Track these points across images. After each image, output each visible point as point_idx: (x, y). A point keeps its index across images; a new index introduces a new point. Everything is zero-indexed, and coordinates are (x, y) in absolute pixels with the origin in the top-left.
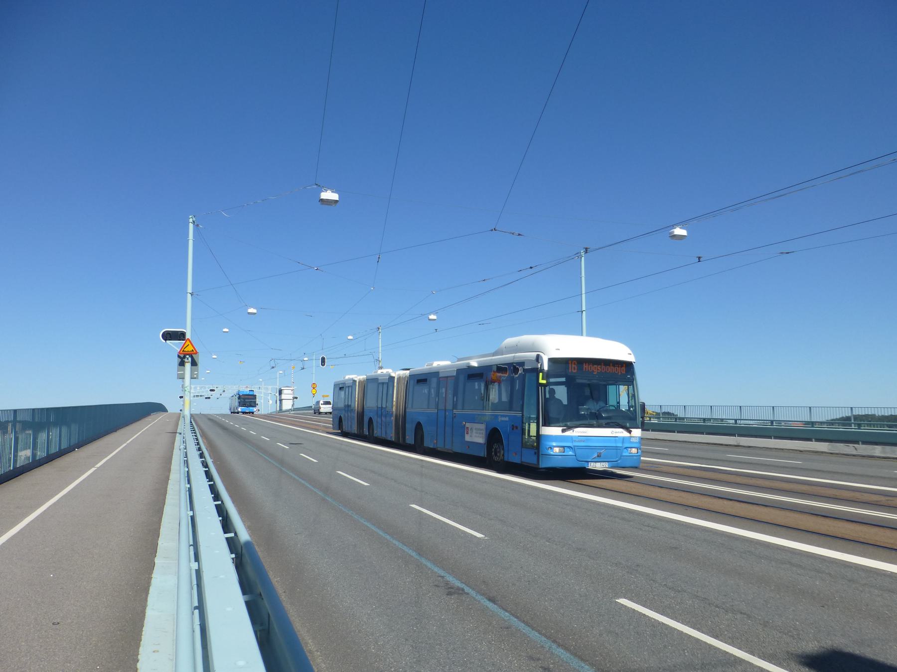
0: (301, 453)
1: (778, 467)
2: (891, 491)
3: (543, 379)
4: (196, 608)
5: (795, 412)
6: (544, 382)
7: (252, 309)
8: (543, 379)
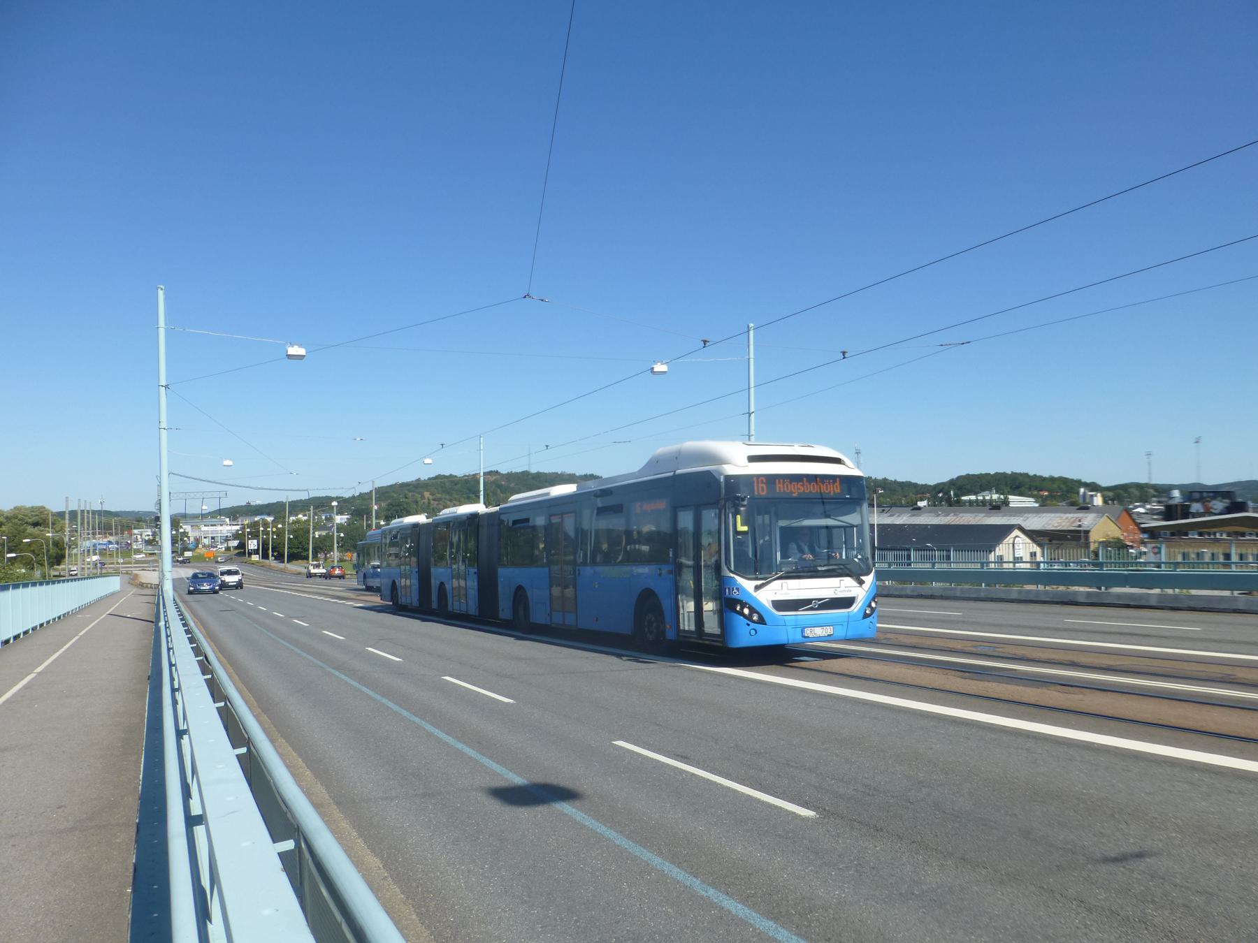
0: (324, 630)
1: (894, 617)
2: (1185, 654)
3: (742, 525)
4: (178, 690)
5: (1071, 554)
6: (745, 528)
7: (296, 347)
8: (742, 525)
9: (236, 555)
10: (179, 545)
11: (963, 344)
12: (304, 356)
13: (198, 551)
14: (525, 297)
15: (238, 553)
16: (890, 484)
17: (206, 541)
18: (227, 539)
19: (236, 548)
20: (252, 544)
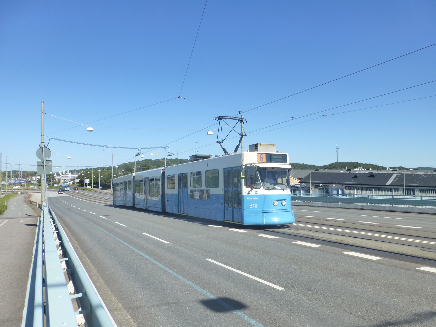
6: (244, 176)
9: (79, 186)
10: (51, 182)
11: (331, 115)
12: (92, 131)
13: (60, 184)
14: (178, 97)
15: (79, 185)
16: (305, 166)
17: (63, 181)
18: (72, 180)
19: (78, 183)
20: (87, 181)
